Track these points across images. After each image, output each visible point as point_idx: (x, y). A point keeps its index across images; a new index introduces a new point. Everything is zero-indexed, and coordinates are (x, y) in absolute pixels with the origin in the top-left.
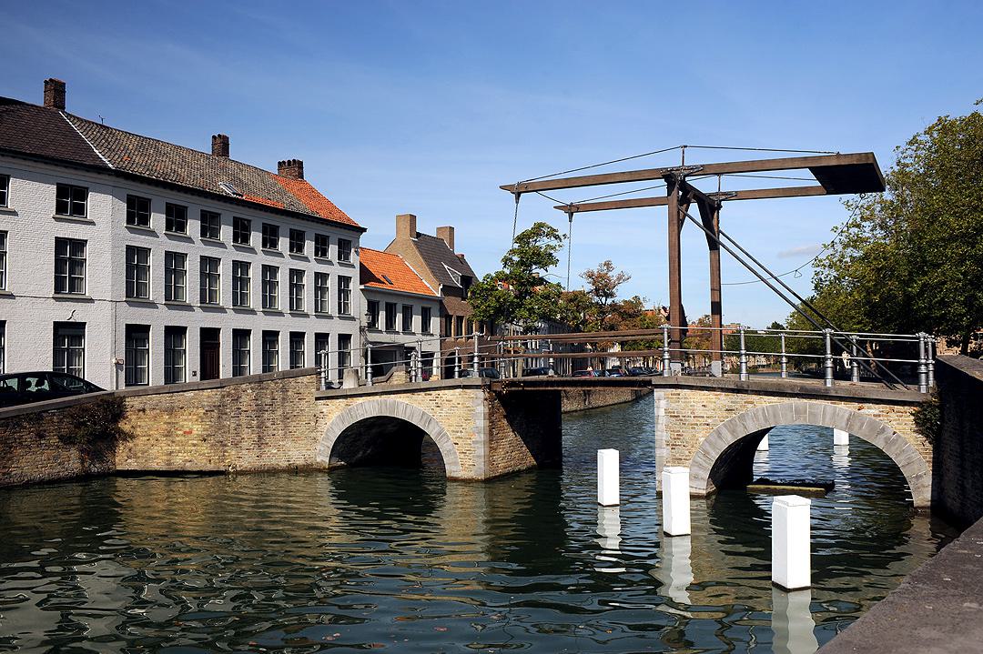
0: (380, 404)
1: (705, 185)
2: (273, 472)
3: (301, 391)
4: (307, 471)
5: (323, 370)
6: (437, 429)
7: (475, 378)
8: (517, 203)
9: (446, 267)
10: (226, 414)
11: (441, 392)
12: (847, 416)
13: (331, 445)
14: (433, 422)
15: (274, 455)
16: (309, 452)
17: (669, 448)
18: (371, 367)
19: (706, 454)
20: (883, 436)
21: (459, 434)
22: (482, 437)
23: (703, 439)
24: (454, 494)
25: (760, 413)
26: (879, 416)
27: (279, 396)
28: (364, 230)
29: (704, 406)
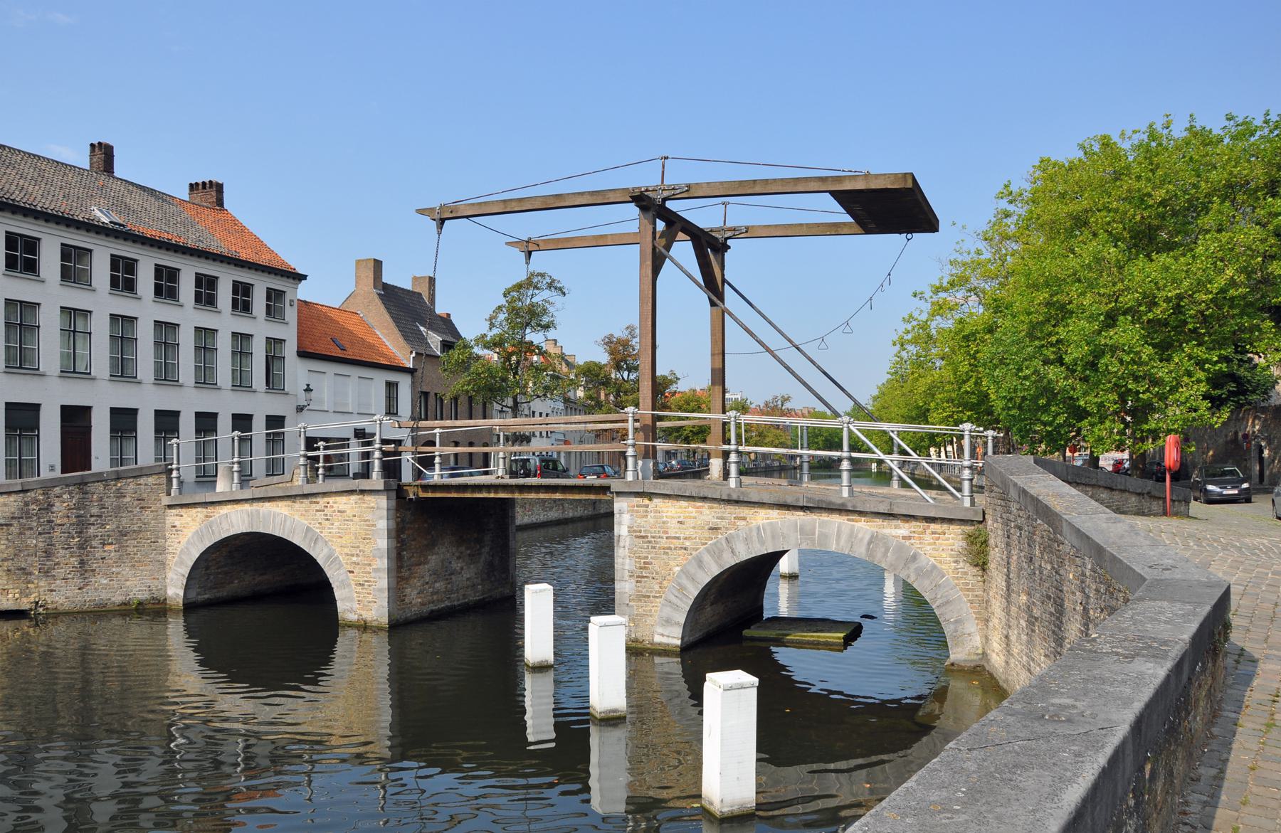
0: (250, 515)
1: (704, 215)
2: (100, 613)
3: (145, 496)
4: (154, 610)
5: (174, 466)
6: (326, 551)
7: (376, 481)
8: (439, 234)
9: (422, 328)
10: (31, 529)
11: (331, 500)
12: (867, 538)
13: (186, 571)
14: (320, 544)
15: (105, 587)
16: (156, 582)
17: (633, 581)
18: (324, 467)
19: (682, 588)
20: (913, 566)
21: (354, 559)
22: (383, 563)
23: (678, 569)
24: (345, 644)
25: (754, 533)
26: (910, 538)
27: (110, 502)
28: (304, 277)
29: (680, 522)
